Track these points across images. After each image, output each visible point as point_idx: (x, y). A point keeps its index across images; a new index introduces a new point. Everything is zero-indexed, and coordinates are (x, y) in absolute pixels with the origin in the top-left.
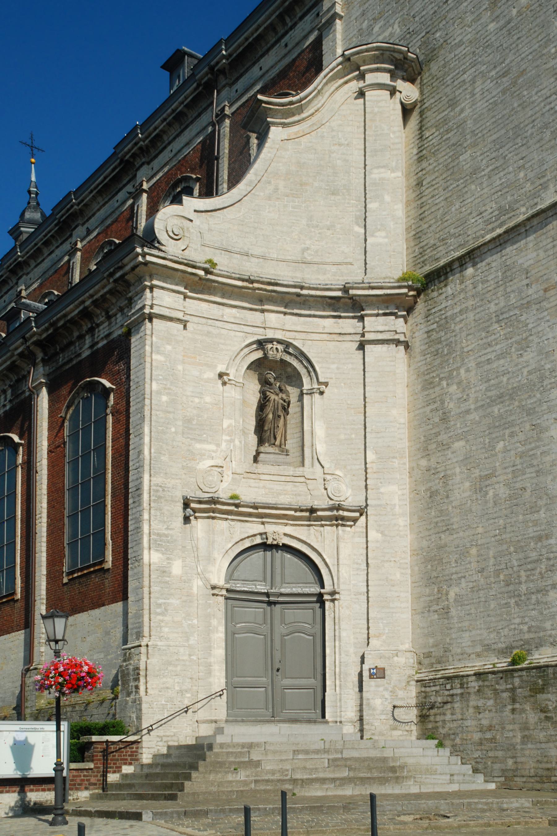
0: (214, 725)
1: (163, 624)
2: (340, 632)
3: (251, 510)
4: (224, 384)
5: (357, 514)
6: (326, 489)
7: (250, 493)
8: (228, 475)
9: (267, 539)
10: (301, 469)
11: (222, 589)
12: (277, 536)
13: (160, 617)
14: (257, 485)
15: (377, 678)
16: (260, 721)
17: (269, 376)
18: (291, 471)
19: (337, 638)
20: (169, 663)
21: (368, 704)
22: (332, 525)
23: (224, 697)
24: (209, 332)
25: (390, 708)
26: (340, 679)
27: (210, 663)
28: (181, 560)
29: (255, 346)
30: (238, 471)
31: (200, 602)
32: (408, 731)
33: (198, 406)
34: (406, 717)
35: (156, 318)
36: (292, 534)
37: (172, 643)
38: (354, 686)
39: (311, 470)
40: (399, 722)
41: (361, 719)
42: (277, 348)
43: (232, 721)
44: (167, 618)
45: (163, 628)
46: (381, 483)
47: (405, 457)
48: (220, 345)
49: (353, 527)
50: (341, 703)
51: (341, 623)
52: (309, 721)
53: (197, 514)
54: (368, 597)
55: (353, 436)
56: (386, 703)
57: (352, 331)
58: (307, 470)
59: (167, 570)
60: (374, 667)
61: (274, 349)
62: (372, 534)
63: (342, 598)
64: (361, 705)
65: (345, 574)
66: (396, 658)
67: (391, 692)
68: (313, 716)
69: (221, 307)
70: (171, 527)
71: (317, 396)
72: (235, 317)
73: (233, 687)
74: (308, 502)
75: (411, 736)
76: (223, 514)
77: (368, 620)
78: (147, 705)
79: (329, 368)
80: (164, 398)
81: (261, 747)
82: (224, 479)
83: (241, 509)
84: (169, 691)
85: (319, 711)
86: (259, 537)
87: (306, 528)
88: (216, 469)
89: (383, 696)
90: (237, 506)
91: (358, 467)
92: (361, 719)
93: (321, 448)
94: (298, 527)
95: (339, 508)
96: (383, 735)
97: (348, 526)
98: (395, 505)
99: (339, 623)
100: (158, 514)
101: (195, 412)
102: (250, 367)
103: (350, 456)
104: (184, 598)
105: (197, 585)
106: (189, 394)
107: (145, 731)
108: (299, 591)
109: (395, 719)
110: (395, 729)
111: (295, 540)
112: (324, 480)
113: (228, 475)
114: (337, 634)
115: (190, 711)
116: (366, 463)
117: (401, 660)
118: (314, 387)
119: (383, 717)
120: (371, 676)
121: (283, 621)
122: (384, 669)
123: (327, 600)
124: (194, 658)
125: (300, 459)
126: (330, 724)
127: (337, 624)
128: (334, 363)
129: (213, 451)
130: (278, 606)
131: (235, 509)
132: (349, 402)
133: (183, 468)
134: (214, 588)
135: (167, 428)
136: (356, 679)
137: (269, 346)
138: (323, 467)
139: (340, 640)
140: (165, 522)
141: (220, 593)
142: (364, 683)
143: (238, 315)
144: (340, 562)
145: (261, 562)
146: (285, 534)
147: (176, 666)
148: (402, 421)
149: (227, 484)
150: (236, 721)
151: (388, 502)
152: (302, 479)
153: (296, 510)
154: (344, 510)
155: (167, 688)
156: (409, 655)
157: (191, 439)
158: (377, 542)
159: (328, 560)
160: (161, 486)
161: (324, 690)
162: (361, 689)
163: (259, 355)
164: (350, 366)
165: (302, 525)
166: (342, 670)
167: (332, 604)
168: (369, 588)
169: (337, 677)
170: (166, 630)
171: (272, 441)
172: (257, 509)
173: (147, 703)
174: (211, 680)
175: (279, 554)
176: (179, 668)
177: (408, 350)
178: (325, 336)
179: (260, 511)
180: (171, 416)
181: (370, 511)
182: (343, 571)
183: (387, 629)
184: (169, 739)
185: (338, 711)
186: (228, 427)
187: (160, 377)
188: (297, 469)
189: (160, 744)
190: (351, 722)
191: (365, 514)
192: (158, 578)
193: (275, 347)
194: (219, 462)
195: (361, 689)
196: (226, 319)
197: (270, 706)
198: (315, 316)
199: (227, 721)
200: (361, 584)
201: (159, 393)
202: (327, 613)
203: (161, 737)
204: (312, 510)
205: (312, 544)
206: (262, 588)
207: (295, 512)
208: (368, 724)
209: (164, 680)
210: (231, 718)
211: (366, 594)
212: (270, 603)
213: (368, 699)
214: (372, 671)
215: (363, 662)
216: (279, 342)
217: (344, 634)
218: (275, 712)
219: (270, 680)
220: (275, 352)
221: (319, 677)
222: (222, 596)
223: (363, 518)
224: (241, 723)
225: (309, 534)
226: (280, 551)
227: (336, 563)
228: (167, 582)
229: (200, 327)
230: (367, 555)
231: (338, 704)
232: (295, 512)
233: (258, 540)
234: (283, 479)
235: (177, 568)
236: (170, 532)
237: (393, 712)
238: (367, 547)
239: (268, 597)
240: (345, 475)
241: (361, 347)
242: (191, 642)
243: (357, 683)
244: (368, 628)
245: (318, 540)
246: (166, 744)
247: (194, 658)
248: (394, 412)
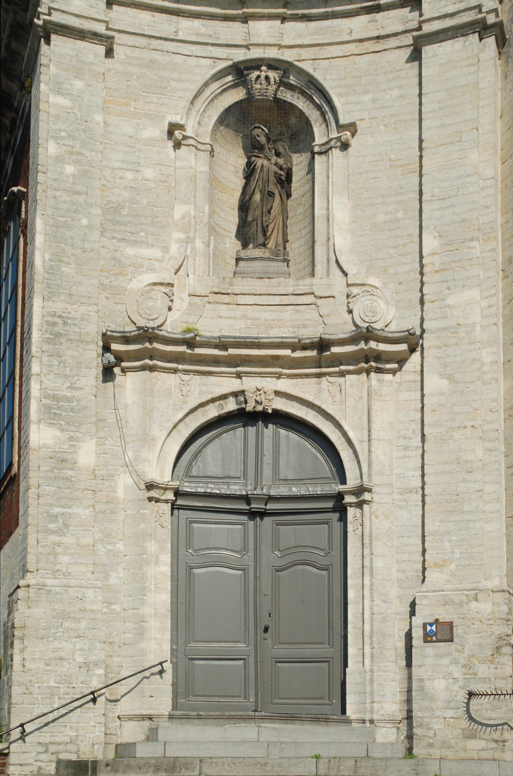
0: (147, 724)
1: (59, 550)
2: (371, 560)
4: (177, 145)
5: (404, 347)
6: (350, 312)
7: (216, 323)
8: (181, 299)
9: (246, 402)
10: (308, 281)
11: (166, 489)
13: (56, 538)
14: (231, 314)
15: (438, 641)
16: (230, 718)
17: (257, 131)
18: (289, 285)
19: (367, 571)
20: (66, 616)
21: (422, 689)
22: (358, 372)
23: (168, 676)
24: (152, 61)
25: (462, 696)
26: (371, 644)
28: (94, 442)
29: (230, 78)
30: (200, 291)
31: (129, 512)
32: (497, 741)
33: (132, 185)
34: (494, 715)
35: (56, 33)
37: (73, 582)
39: (325, 281)
40: (480, 724)
41: (409, 717)
42: (267, 78)
44: (67, 540)
45: (60, 557)
46: (448, 288)
47: (495, 238)
48: (172, 83)
49: (398, 374)
50: (372, 688)
51: (375, 543)
54: (423, 496)
55: (400, 214)
56: (455, 688)
57: (400, 28)
58: (318, 284)
59: (69, 457)
60: (432, 620)
61: (263, 78)
62: (432, 382)
63: (376, 498)
64: (409, 691)
65: (382, 457)
66: (473, 604)
67: (464, 666)
68: (326, 709)
69: (174, 18)
70: (79, 384)
71: (336, 153)
72: (198, 35)
74: (312, 332)
75: (503, 751)
77: (423, 537)
78: (23, 689)
79: (358, 103)
80: (70, 169)
81: (193, 770)
83: (197, 351)
84: (65, 663)
85: (337, 701)
86: (232, 399)
87: (314, 380)
88: (163, 289)
89: (450, 674)
90: (191, 344)
91: (406, 268)
93: (342, 241)
94: (300, 380)
96: (449, 747)
98: (474, 324)
99: (371, 544)
100: (55, 362)
101: (126, 194)
102: (224, 119)
103: (393, 251)
104: (99, 507)
105: (124, 485)
106: (116, 165)
107: (15, 734)
108: (303, 492)
109: (471, 718)
110: (471, 736)
111: (295, 403)
112: (348, 296)
113: (181, 299)
114: (367, 563)
115: (101, 700)
116: (421, 257)
117: (484, 607)
118: (331, 136)
119: (450, 713)
120: (427, 638)
122: (450, 625)
123: (351, 505)
125: (309, 269)
126: (354, 725)
127: (366, 545)
128: (367, 92)
129: (157, 260)
131: (191, 353)
132: (393, 156)
133: (102, 287)
134: (150, 486)
135: (73, 219)
136: (401, 644)
137: (255, 74)
138: (346, 274)
139: (371, 575)
140: (66, 377)
141: (163, 498)
142: (414, 650)
143: (203, 30)
144: (374, 436)
145: (240, 444)
146: (277, 393)
147: (79, 620)
148: (490, 173)
149: (178, 314)
150: (187, 717)
151: (461, 322)
152: (310, 299)
153: (294, 347)
155: (61, 659)
156: (499, 597)
157: (119, 240)
158: (441, 394)
159: (351, 434)
160: (60, 317)
161: (346, 665)
162: (409, 664)
163: (237, 95)
164: (396, 92)
165: (307, 376)
167: (358, 511)
168: (426, 478)
170: (66, 559)
171: (261, 240)
173: (21, 684)
174: (143, 645)
175: (269, 431)
176: (83, 624)
177: (505, 50)
178: (352, 48)
179: (232, 351)
180: (81, 199)
181: (428, 341)
182: (380, 452)
183: (458, 551)
184: (61, 748)
185: (368, 701)
186: (183, 217)
187: (63, 134)
188: (300, 282)
189: (43, 757)
190: (392, 721)
191: (419, 349)
192: (51, 471)
193: (263, 74)
194: (167, 277)
195: (409, 664)
196: (181, 36)
197: (252, 692)
198: (334, 16)
199: (171, 717)
200: (411, 473)
201: (60, 160)
202: (350, 528)
203: (46, 745)
204: (322, 345)
205: (324, 407)
207: (293, 351)
208: (421, 725)
209: (56, 644)
210: (178, 713)
212: (253, 515)
213: (421, 680)
214: (429, 628)
215: (412, 613)
216: (273, 64)
217: (379, 564)
219: (252, 647)
220: (265, 84)
221: (338, 641)
222: (166, 501)
223: (416, 357)
224: (196, 721)
225: (320, 391)
226: (270, 426)
227: (366, 438)
228: (68, 479)
229: (137, 53)
231: (368, 689)
232: (293, 351)
233: (231, 405)
234: (277, 300)
235: (86, 454)
236: (77, 393)
237: (468, 704)
238: (423, 408)
239: (249, 503)
240: (385, 284)
241: (416, 56)
242: (113, 581)
243: (402, 652)
244: (424, 551)
245: (338, 399)
246: (54, 758)
247: (117, 608)
248: (474, 156)
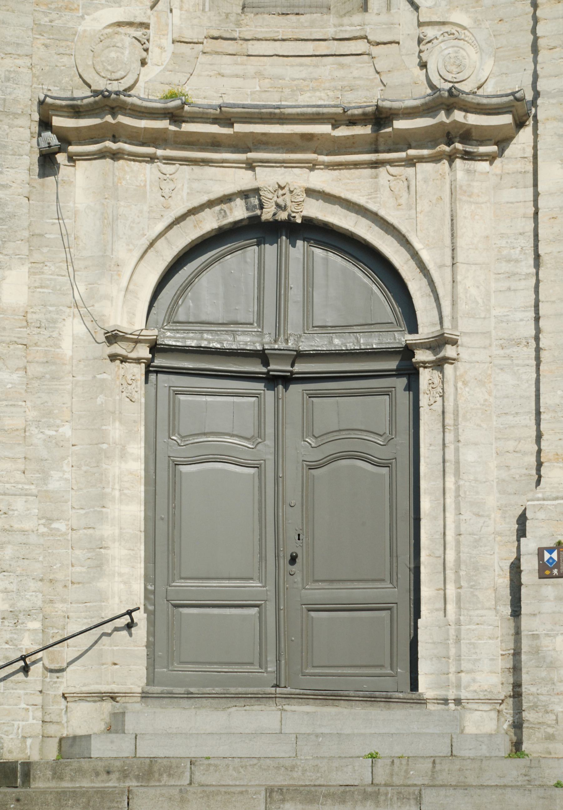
0: (108, 706)
2: (457, 450)
3: (215, 129)
5: (507, 119)
6: (423, 65)
8: (161, 48)
9: (262, 207)
10: (357, 18)
12: (288, 197)
14: (238, 70)
16: (237, 697)
21: (536, 651)
22: (435, 159)
23: (141, 631)
26: (457, 581)
27: (102, 539)
28: (25, 269)
30: (188, 35)
31: (79, 378)
36: (328, 190)
38: (497, 600)
39: (384, 18)
41: (517, 693)
43: (160, 697)
49: (498, 161)
50: (459, 649)
51: (462, 424)
52: (371, 699)
53: (72, 149)
54: (538, 350)
60: (551, 543)
63: (464, 354)
64: (517, 653)
65: (473, 291)
68: (388, 683)
73: (167, 603)
76: (143, 144)
77: (538, 413)
82: (152, 58)
83: (187, 127)
85: (404, 671)
86: (239, 202)
87: (368, 172)
92: (517, 693)
94: (345, 173)
95: (450, 101)
97: (482, 157)
99: (456, 425)
104: (35, 369)
105: (73, 336)
111: (337, 208)
112: (420, 41)
113: (161, 48)
114: (450, 455)
115: (36, 670)
120: (545, 571)
121: (308, 429)
123: (425, 365)
124: (61, 526)
126: (431, 707)
130: (296, 389)
131: (179, 130)
133: (38, 28)
134: (113, 338)
136: (504, 581)
139: (457, 473)
141: (133, 355)
144: (461, 257)
145: (252, 272)
146: (310, 192)
149: (157, 70)
150: (171, 696)
154: (468, 108)
159: (425, 255)
161: (417, 614)
165: (356, 165)
166: (463, 556)
167: (436, 374)
169: (450, 574)
172: (231, 125)
174: (102, 584)
181: (544, 110)
182: (468, 280)
185: (453, 669)
188: (346, 20)
190: (489, 701)
191: (531, 122)
195: (516, 613)
197: (271, 657)
199: (145, 696)
200: (519, 315)
202: (424, 401)
204: (380, 118)
205: (382, 213)
206: (246, 341)
207: (335, 127)
208: (535, 707)
210: (157, 689)
211: (533, 344)
212: (273, 381)
213: (535, 637)
214: (547, 556)
215: (522, 533)
217: (469, 456)
218: (293, 673)
219: (271, 587)
221: (405, 577)
222: (138, 361)
223: (526, 134)
224: (185, 702)
225: (376, 189)
226: (299, 243)
227: (449, 262)
230: (536, 235)
231: (453, 651)
233: (238, 212)
234: (309, 48)
238: (536, 213)
239: (266, 363)
244: (539, 437)
245: (403, 200)
247: (61, 526)
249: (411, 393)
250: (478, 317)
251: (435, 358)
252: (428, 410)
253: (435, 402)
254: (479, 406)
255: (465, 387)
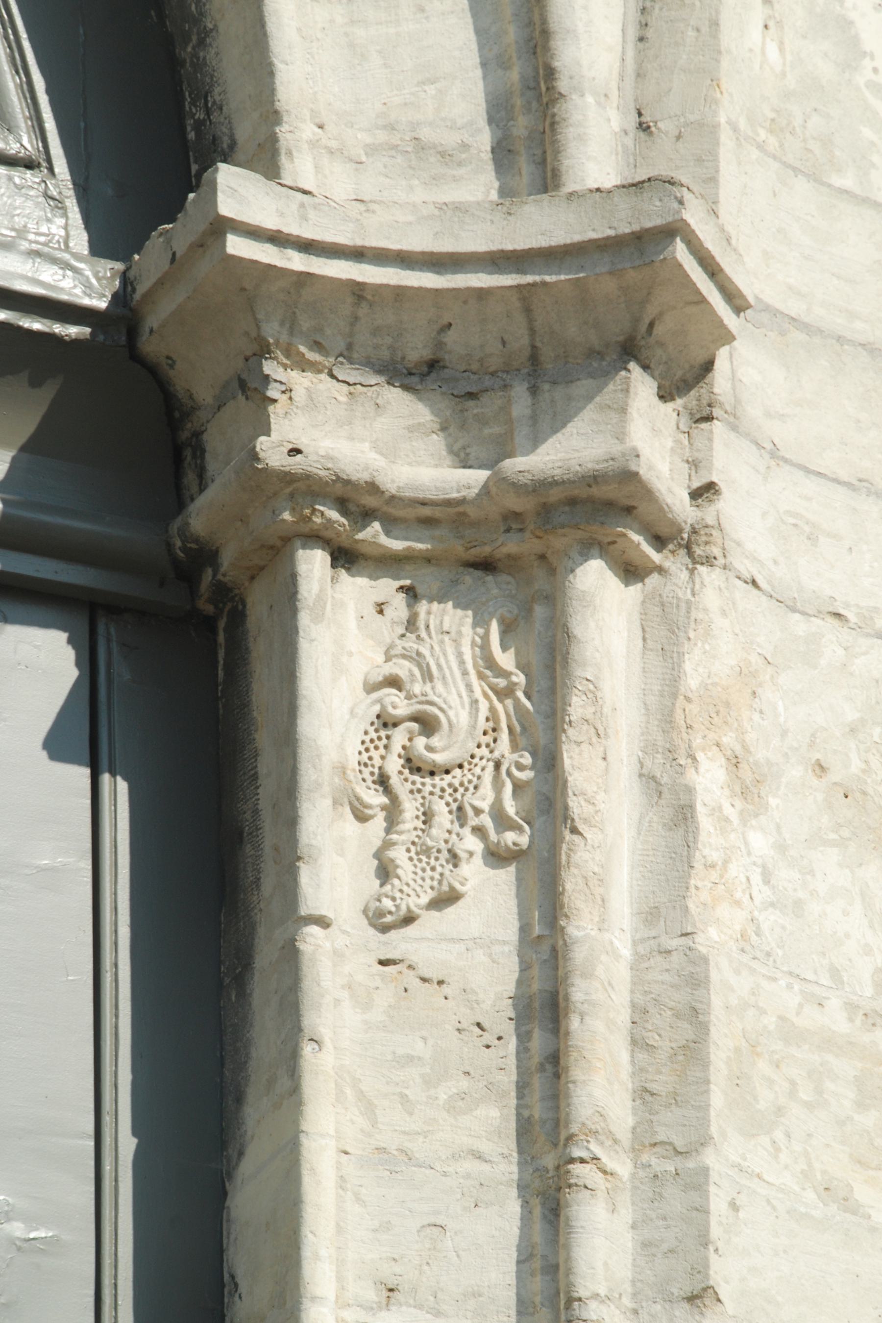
123: (353, 519)
167: (457, 638)
249: (118, 792)
250: (847, 182)
251: (475, 478)
252: (361, 967)
253: (446, 899)
254: (835, 1019)
255: (744, 817)
